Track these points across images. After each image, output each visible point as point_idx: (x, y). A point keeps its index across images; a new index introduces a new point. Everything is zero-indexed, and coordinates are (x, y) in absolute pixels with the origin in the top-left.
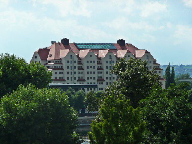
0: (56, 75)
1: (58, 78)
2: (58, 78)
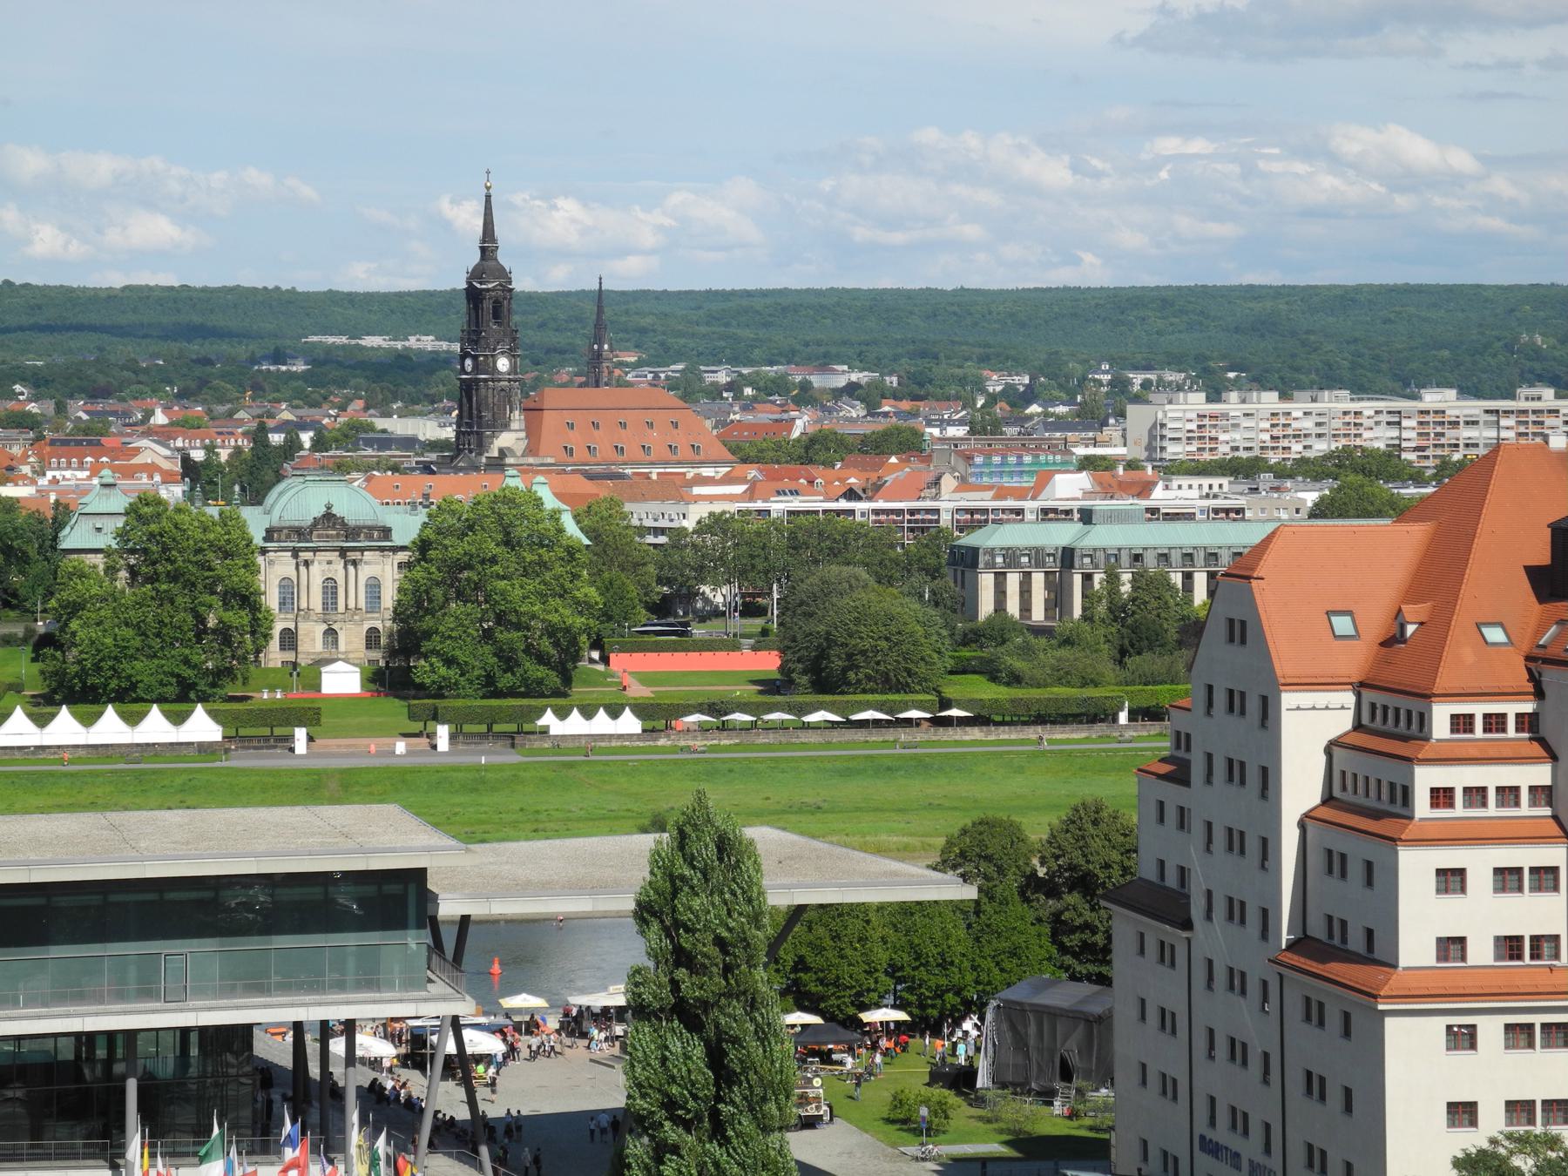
0: (1451, 915)
1: (1481, 953)
2: (1481, 953)
